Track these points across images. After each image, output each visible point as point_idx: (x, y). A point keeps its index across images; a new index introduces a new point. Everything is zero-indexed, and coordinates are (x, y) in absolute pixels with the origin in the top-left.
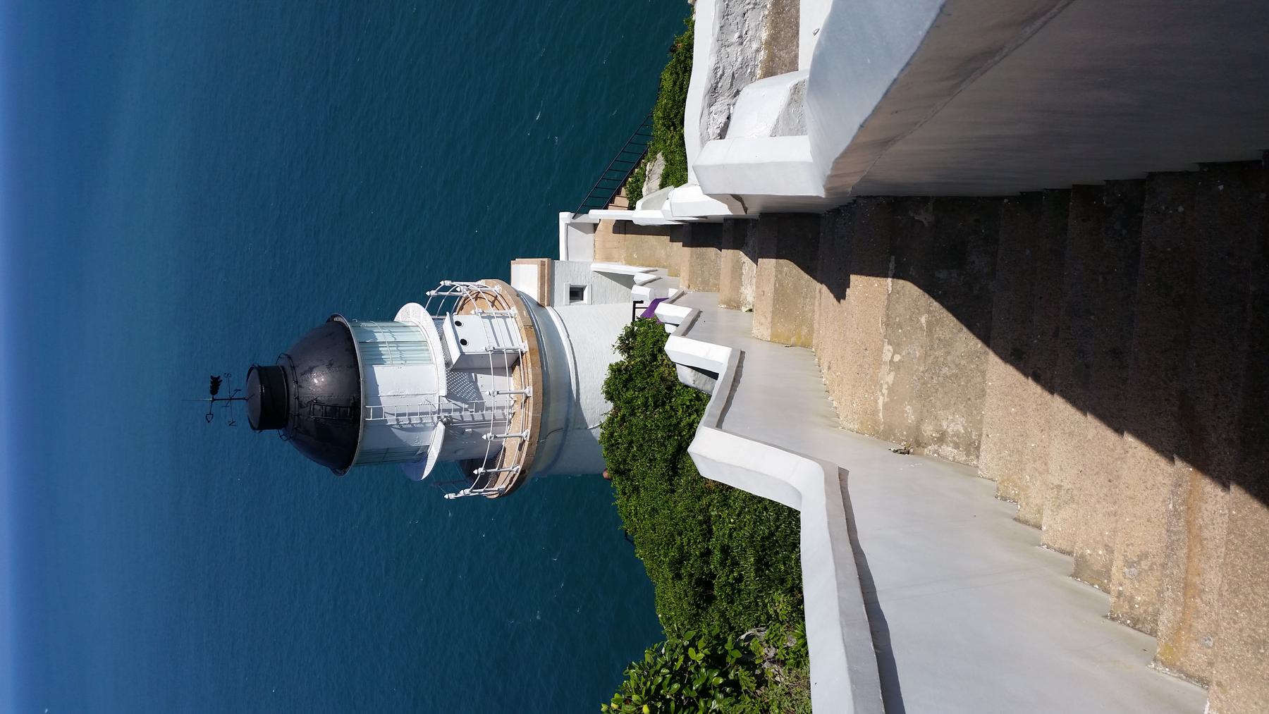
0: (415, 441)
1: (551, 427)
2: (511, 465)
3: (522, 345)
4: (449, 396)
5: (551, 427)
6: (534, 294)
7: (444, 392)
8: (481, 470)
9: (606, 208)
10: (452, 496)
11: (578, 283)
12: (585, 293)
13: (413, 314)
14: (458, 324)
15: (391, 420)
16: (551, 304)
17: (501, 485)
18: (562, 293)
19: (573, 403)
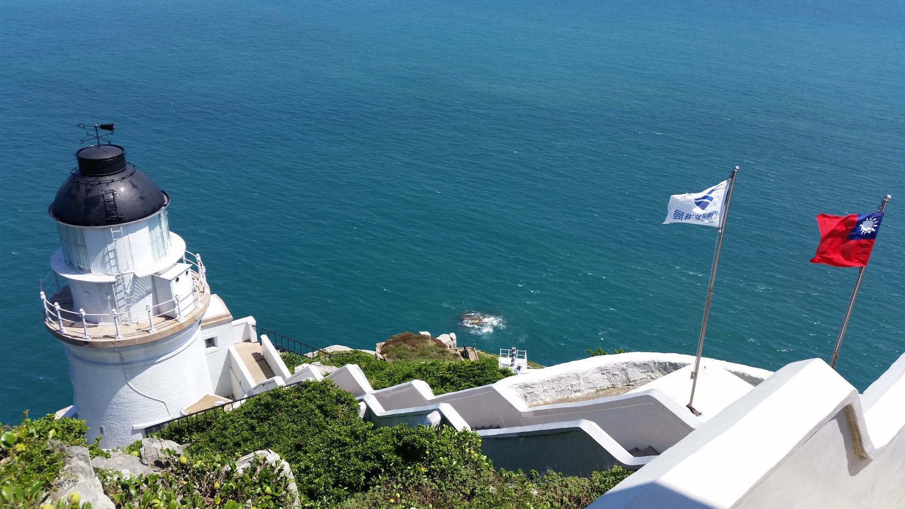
1: (124, 354)
2: (88, 333)
3: (182, 319)
5: (124, 354)
9: (277, 348)
10: (43, 296)
11: (219, 342)
12: (212, 348)
15: (110, 247)
16: (203, 328)
17: (68, 331)
18: (210, 333)
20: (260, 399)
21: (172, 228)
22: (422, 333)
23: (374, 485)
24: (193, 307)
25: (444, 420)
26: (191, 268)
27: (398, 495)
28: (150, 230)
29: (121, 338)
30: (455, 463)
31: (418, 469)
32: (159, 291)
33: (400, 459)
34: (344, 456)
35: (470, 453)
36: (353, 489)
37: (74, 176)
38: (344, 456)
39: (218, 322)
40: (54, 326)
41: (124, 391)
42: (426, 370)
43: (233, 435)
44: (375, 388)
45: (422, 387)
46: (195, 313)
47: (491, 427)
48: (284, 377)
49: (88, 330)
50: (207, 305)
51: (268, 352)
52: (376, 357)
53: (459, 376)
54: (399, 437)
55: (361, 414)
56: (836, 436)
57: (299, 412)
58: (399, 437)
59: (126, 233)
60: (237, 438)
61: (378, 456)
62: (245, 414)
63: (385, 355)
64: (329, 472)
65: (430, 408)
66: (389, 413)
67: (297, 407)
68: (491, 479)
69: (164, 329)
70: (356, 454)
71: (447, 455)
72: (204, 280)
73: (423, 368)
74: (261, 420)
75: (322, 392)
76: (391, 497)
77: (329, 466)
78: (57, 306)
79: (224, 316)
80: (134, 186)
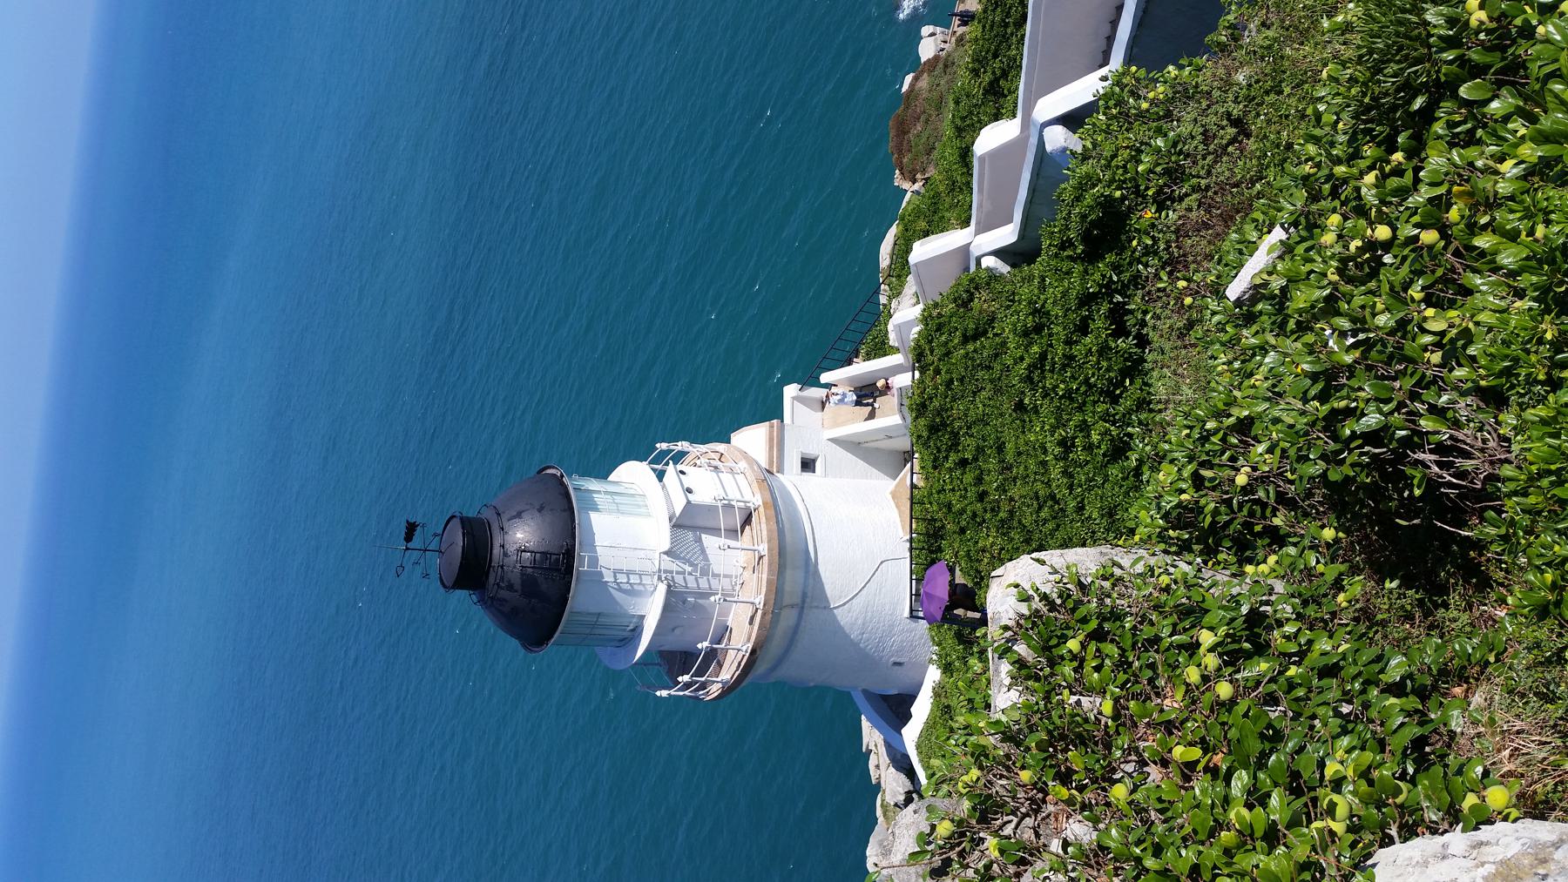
0: (634, 607)
1: (787, 600)
3: (756, 499)
5: (787, 600)
8: (706, 644)
9: (850, 363)
10: (664, 693)
11: (811, 451)
12: (818, 464)
14: (682, 472)
15: (608, 577)
16: (781, 470)
17: (727, 673)
20: (919, 437)
21: (603, 475)
22: (905, 88)
23: (1143, 324)
24: (740, 478)
25: (1072, 120)
26: (675, 463)
27: (1182, 284)
28: (597, 510)
29: (760, 600)
30: (1160, 142)
31: (1144, 224)
32: (700, 523)
33: (1110, 258)
34: (1064, 367)
35: (1152, 102)
36: (1134, 368)
37: (481, 601)
38: (1064, 367)
39: (777, 445)
40: (715, 690)
41: (844, 617)
42: (963, 119)
43: (965, 497)
44: (966, 223)
45: (993, 137)
46: (751, 477)
47: (1115, 24)
48: (897, 370)
49: (733, 644)
50: (745, 455)
51: (851, 380)
52: (917, 193)
53: (995, 56)
54: (1063, 246)
55: (1004, 268)
56: (680, 532)
57: (961, 380)
58: (1063, 246)
59: (593, 547)
60: (972, 492)
61: (1087, 300)
62: (935, 468)
63: (919, 176)
64: (1084, 403)
65: (1034, 141)
66: (1018, 216)
67: (951, 381)
68: (1221, 71)
69: (765, 533)
70: (1069, 343)
71: (1139, 151)
72: (703, 448)
73: (958, 122)
74: (954, 445)
75: (939, 328)
76: (1179, 299)
77: (1072, 400)
78: (686, 678)
79: (771, 433)
80: (519, 515)
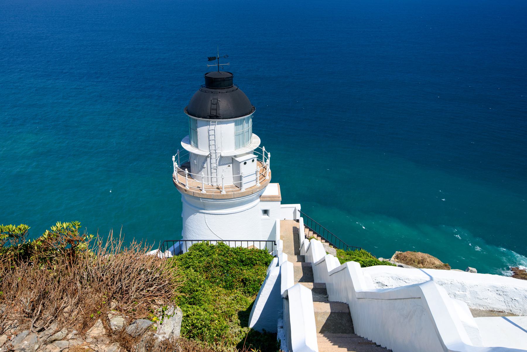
4: (221, 157)
6: (264, 194)
7: (222, 155)
10: (174, 159)
11: (270, 213)
13: (256, 141)
14: (253, 161)
16: (261, 201)
18: (266, 206)
19: (194, 142)
39: (271, 199)
